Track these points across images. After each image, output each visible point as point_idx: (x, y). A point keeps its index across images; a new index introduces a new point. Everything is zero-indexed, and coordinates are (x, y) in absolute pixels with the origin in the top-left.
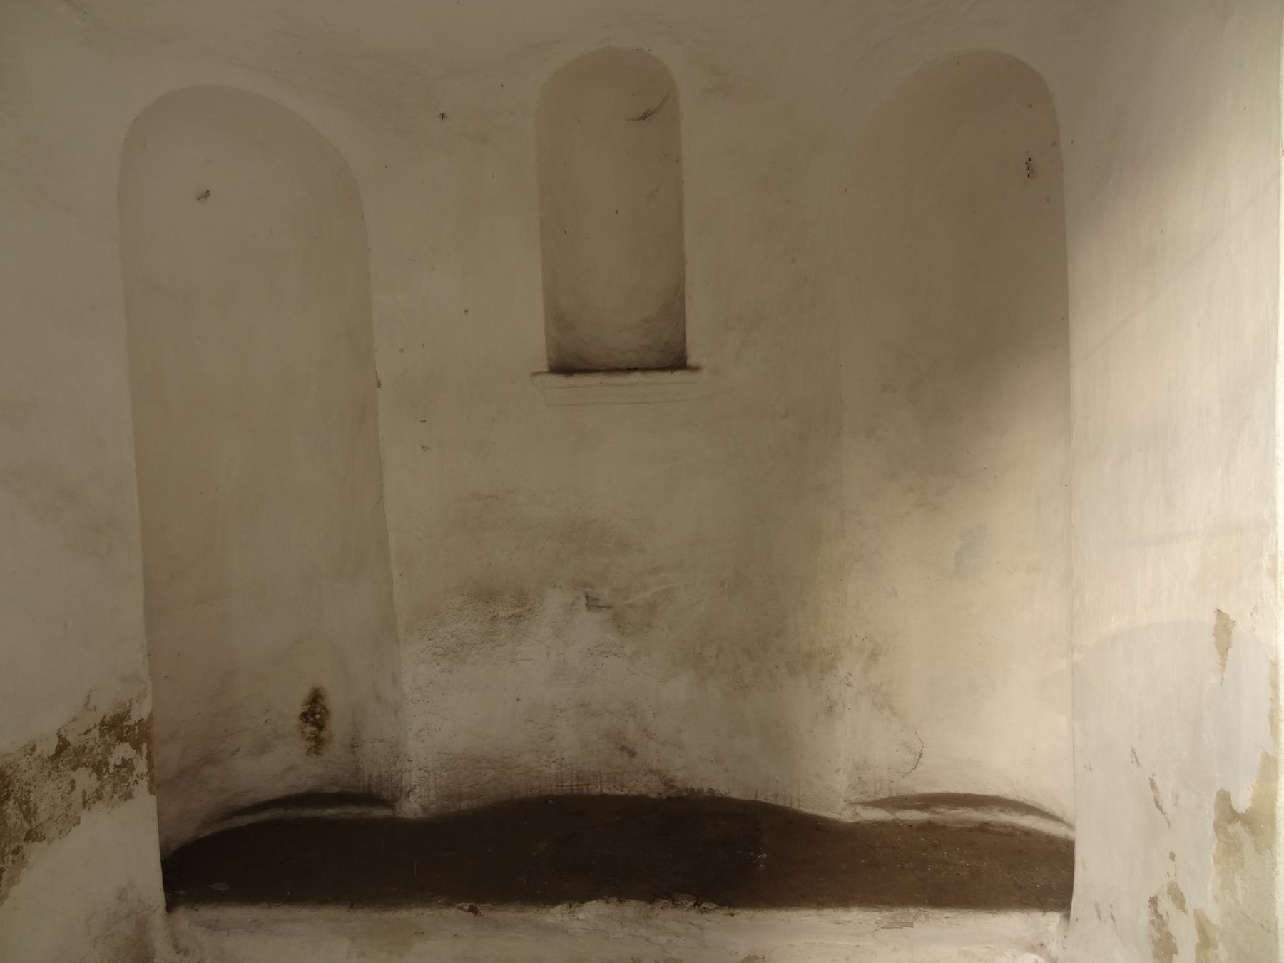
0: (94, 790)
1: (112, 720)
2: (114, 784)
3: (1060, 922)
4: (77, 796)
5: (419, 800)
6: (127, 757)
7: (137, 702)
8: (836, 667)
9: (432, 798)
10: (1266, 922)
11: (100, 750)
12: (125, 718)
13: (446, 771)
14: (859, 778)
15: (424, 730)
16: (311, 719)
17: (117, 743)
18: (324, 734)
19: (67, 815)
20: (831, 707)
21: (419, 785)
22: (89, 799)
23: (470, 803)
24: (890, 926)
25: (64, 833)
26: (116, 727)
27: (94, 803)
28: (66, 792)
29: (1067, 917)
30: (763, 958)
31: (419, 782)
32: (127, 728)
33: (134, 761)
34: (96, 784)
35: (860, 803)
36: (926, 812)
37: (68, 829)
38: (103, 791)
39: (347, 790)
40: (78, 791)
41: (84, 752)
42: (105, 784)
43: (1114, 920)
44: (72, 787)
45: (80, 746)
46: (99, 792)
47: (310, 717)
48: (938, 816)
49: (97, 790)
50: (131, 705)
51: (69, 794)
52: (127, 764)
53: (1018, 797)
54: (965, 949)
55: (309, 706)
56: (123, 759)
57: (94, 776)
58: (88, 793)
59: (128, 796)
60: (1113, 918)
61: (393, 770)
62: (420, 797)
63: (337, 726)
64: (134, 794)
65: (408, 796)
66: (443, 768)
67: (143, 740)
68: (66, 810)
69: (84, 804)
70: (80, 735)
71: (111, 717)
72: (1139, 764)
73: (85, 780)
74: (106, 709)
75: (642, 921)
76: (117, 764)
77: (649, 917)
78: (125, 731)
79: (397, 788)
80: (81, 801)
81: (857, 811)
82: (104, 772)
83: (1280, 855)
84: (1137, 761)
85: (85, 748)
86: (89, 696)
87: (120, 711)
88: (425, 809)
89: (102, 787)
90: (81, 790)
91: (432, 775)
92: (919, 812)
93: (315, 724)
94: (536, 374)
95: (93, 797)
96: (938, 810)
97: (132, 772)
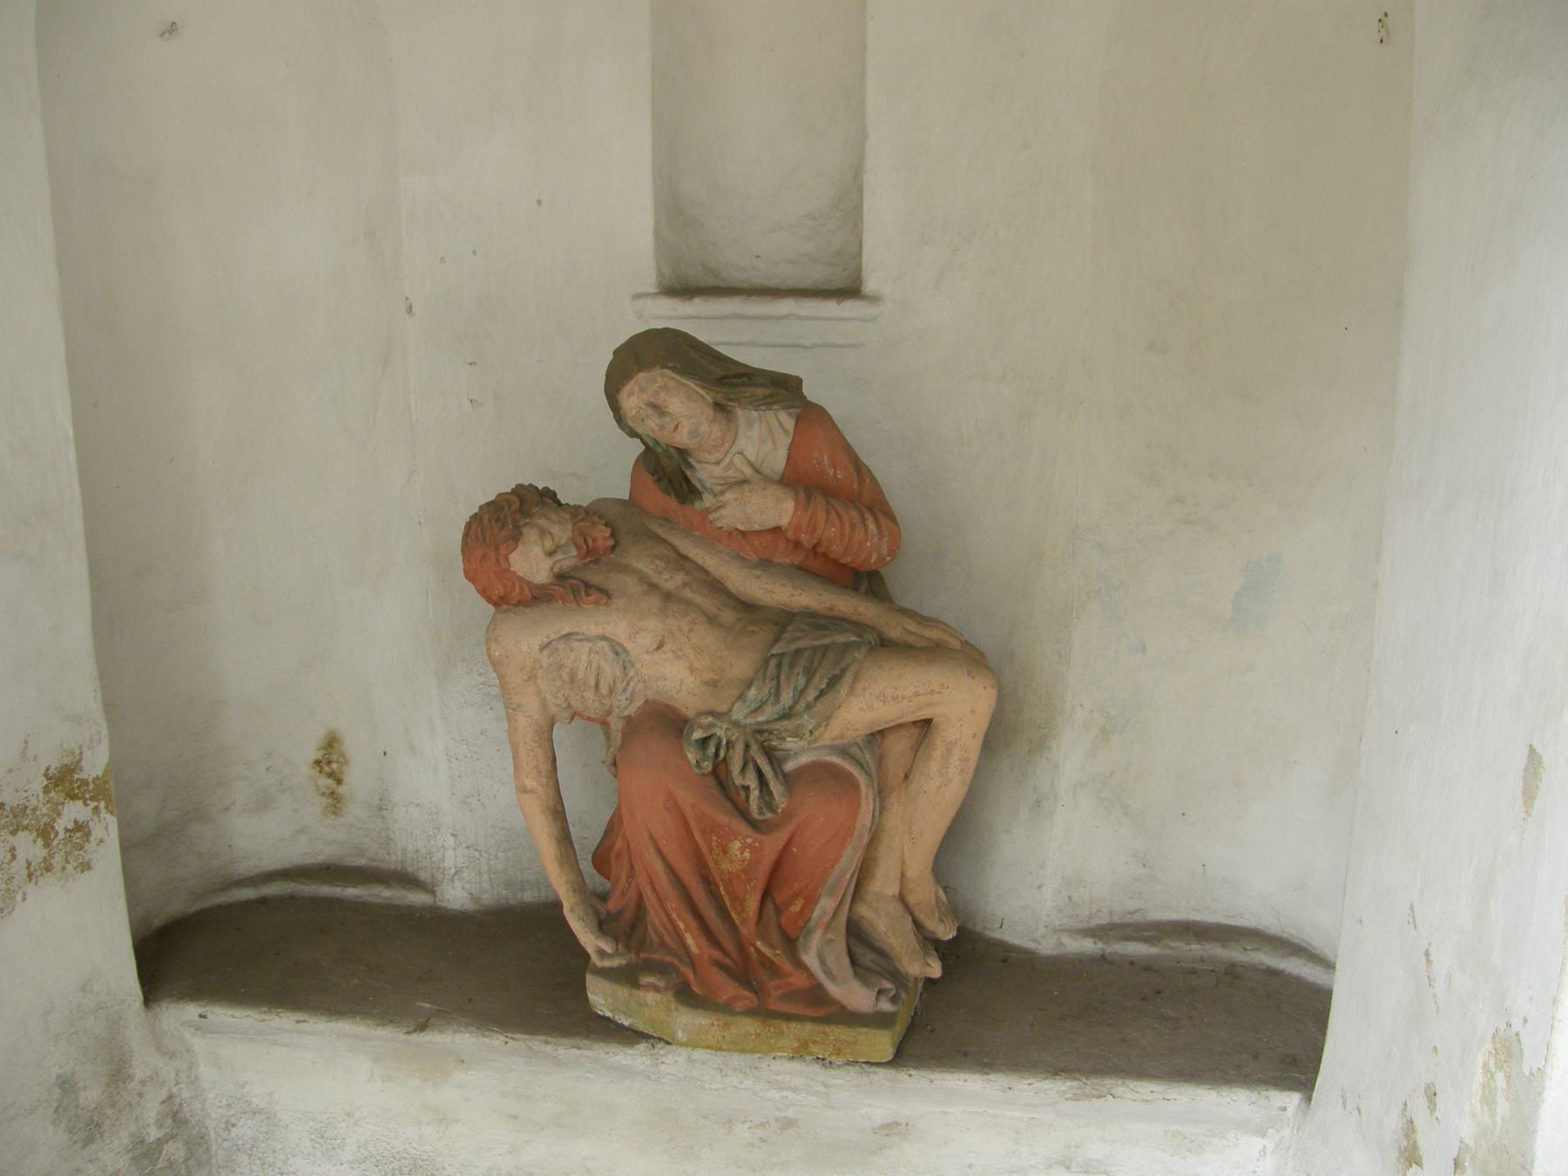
0: (41, 860)
1: (59, 772)
2: (66, 852)
3: (1300, 1104)
4: (19, 867)
5: (468, 887)
6: (81, 819)
7: (89, 749)
8: (1049, 748)
9: (486, 885)
10: (1523, 1156)
11: (44, 811)
12: (75, 769)
13: (504, 851)
14: (1069, 897)
15: (472, 796)
16: (326, 769)
17: (66, 802)
18: (341, 790)
19: (8, 890)
20: (1038, 801)
21: (467, 867)
22: (35, 870)
23: (536, 895)
24: (1076, 1098)
25: (6, 911)
26: (64, 781)
27: (42, 875)
28: (6, 861)
29: (1309, 1099)
30: (907, 1125)
31: (467, 864)
32: (79, 782)
33: (91, 823)
34: (43, 853)
35: (1067, 931)
36: (1156, 946)
37: (11, 906)
38: (52, 861)
39: (375, 864)
40: (20, 862)
41: (24, 812)
42: (55, 853)
43: (1360, 1113)
44: (12, 855)
45: (18, 805)
46: (48, 863)
47: (324, 766)
48: (1172, 952)
49: (45, 860)
50: (81, 753)
51: (9, 864)
52: (80, 827)
53: (1283, 931)
54: (1174, 1128)
55: (323, 751)
56: (76, 821)
57: (40, 842)
58: (34, 864)
59: (86, 866)
60: (1359, 1110)
61: (432, 846)
62: (469, 882)
63: (357, 779)
64: (92, 865)
65: (452, 880)
66: (500, 846)
67: (101, 797)
68: (7, 884)
69: (30, 876)
70: (17, 791)
71: (56, 768)
72: (1415, 927)
73: (29, 847)
74: (53, 760)
75: (748, 1071)
76: (68, 827)
77: (757, 1068)
78: (75, 786)
79: (438, 868)
80: (25, 872)
81: (1062, 940)
82: (52, 836)
83: (1550, 1079)
84: (1414, 921)
85: (26, 807)
86: (26, 742)
87: (66, 761)
88: (475, 899)
89: (51, 856)
90: (25, 861)
91: (484, 855)
92: (1146, 945)
93: (331, 775)
94: (638, 296)
95: (40, 868)
96: (1173, 944)
97: (88, 838)
